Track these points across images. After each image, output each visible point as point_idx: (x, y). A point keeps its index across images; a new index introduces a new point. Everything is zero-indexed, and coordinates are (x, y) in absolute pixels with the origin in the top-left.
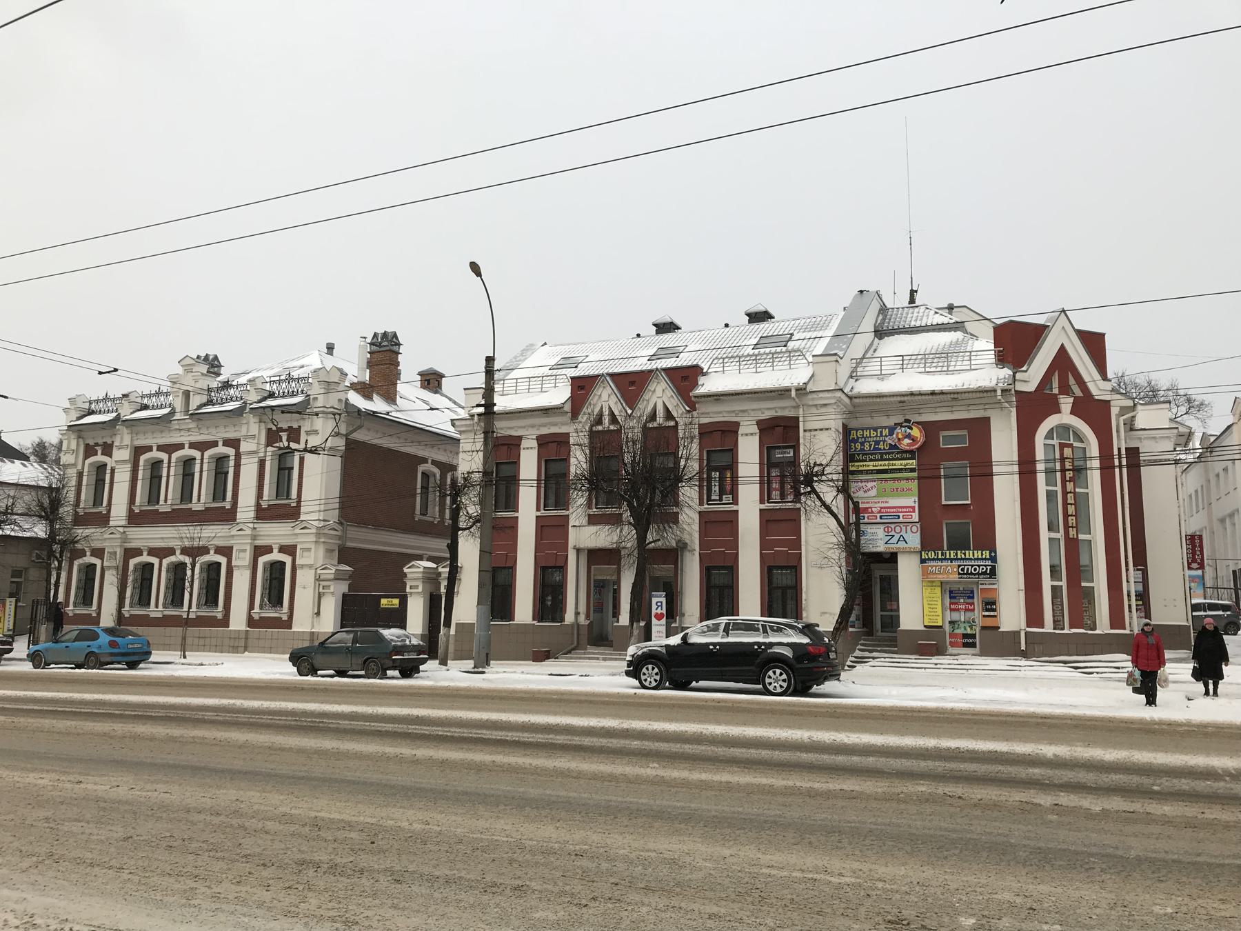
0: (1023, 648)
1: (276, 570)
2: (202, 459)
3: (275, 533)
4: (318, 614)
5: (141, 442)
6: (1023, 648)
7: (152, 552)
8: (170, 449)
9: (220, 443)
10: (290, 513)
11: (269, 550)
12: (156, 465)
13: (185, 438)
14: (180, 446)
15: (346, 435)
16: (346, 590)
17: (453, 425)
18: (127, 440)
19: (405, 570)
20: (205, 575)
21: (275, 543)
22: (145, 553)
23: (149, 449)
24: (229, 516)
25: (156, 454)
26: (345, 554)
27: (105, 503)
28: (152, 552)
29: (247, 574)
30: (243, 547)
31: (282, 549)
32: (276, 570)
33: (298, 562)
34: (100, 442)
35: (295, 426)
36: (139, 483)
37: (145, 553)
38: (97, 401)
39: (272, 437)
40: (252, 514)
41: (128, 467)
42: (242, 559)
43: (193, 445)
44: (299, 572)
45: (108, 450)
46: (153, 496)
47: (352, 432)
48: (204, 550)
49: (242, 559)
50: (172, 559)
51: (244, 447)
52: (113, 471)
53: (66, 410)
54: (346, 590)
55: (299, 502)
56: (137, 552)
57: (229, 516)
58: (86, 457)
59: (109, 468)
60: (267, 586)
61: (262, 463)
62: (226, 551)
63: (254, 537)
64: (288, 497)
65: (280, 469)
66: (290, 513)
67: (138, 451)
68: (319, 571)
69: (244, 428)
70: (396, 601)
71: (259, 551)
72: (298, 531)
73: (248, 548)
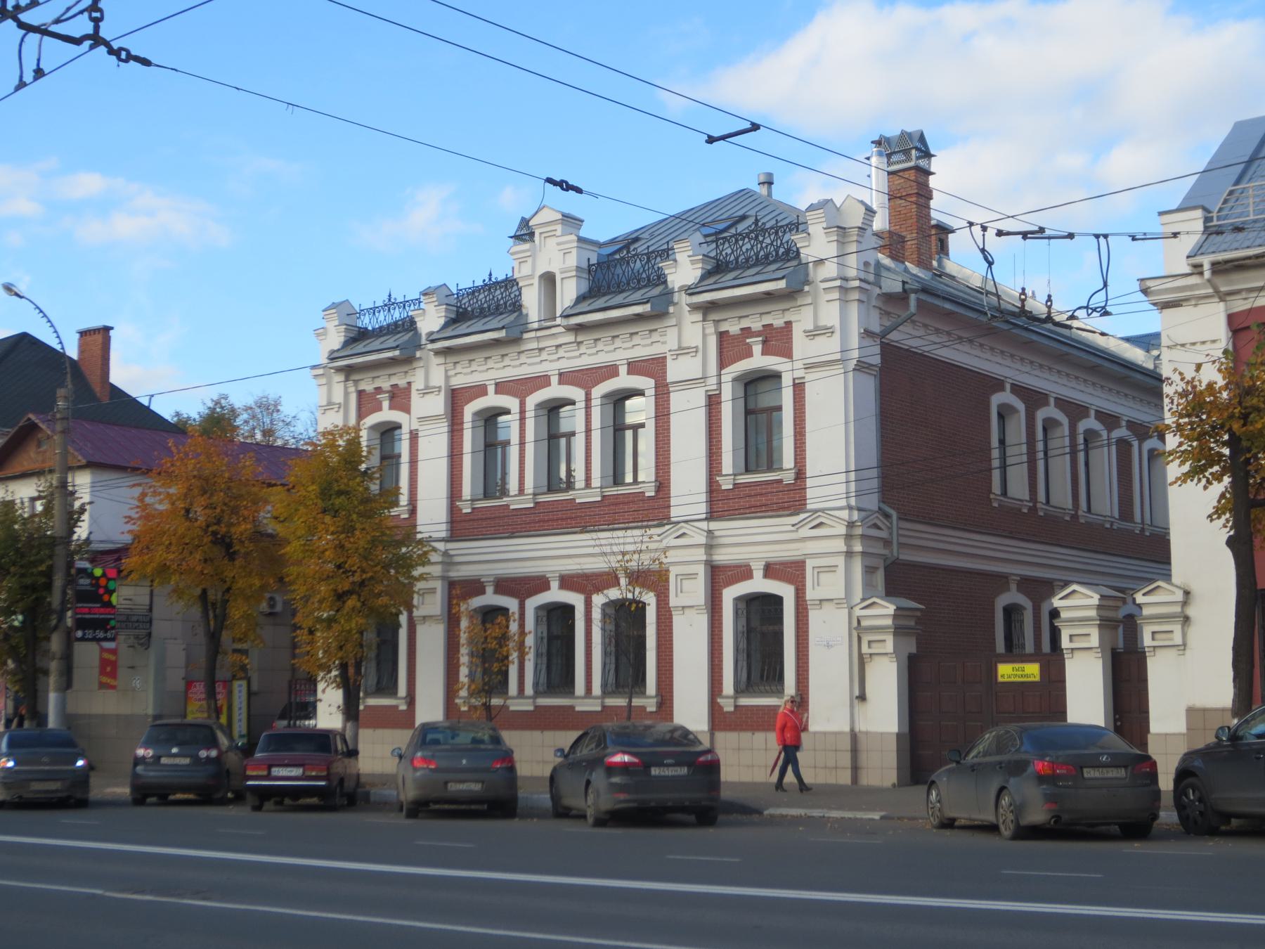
0: (655, 771)
1: (762, 611)
2: (522, 411)
3: (754, 540)
4: (862, 697)
5: (462, 379)
6: (655, 771)
7: (568, 582)
8: (520, 387)
9: (491, 389)
10: (789, 499)
11: (744, 572)
12: (490, 418)
13: (550, 366)
14: (543, 381)
15: (883, 335)
16: (914, 650)
17: (1145, 291)
18: (437, 378)
19: (1140, 598)
20: (544, 628)
21: (756, 557)
22: (490, 590)
23: (481, 391)
24: (652, 509)
25: (492, 400)
26: (896, 578)
27: (788, 460)
28: (568, 582)
29: (703, 621)
30: (431, 584)
31: (771, 571)
32: (762, 611)
33: (810, 594)
34: (756, 325)
35: (778, 322)
36: (467, 461)
37: (490, 590)
38: (374, 310)
39: (730, 348)
40: (703, 508)
41: (443, 427)
42: (689, 592)
43: (566, 378)
44: (814, 617)
45: (400, 398)
46: (492, 483)
47: (894, 328)
48: (540, 584)
49: (689, 592)
50: (614, 594)
51: (675, 370)
52: (414, 437)
53: (321, 333)
54: (914, 650)
55: (800, 474)
56: (475, 587)
57: (652, 509)
58: (722, 364)
59: (787, 381)
60: (743, 645)
61: (713, 403)
62: (655, 579)
63: (709, 547)
64: (772, 463)
65: (748, 412)
66: (789, 499)
67: (457, 399)
68: (858, 612)
69: (672, 335)
70: (1032, 671)
71: (718, 576)
72: (805, 532)
73: (701, 570)
